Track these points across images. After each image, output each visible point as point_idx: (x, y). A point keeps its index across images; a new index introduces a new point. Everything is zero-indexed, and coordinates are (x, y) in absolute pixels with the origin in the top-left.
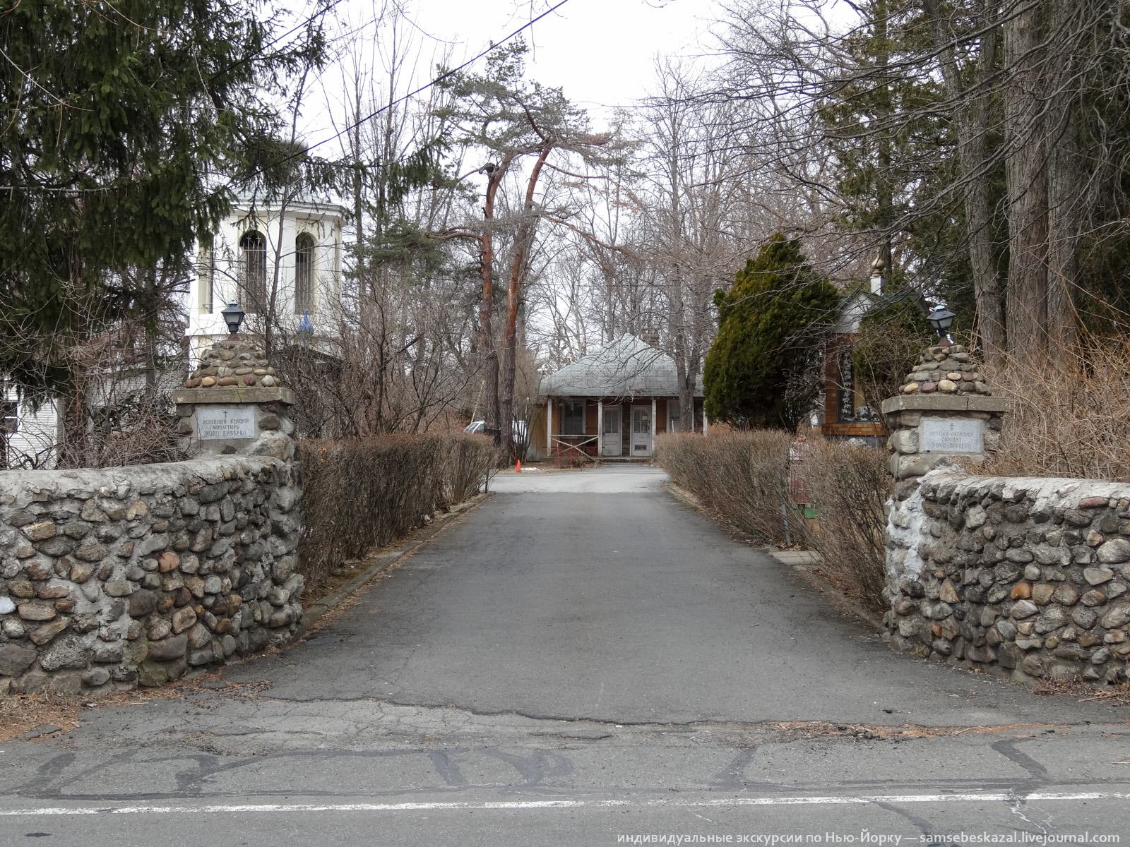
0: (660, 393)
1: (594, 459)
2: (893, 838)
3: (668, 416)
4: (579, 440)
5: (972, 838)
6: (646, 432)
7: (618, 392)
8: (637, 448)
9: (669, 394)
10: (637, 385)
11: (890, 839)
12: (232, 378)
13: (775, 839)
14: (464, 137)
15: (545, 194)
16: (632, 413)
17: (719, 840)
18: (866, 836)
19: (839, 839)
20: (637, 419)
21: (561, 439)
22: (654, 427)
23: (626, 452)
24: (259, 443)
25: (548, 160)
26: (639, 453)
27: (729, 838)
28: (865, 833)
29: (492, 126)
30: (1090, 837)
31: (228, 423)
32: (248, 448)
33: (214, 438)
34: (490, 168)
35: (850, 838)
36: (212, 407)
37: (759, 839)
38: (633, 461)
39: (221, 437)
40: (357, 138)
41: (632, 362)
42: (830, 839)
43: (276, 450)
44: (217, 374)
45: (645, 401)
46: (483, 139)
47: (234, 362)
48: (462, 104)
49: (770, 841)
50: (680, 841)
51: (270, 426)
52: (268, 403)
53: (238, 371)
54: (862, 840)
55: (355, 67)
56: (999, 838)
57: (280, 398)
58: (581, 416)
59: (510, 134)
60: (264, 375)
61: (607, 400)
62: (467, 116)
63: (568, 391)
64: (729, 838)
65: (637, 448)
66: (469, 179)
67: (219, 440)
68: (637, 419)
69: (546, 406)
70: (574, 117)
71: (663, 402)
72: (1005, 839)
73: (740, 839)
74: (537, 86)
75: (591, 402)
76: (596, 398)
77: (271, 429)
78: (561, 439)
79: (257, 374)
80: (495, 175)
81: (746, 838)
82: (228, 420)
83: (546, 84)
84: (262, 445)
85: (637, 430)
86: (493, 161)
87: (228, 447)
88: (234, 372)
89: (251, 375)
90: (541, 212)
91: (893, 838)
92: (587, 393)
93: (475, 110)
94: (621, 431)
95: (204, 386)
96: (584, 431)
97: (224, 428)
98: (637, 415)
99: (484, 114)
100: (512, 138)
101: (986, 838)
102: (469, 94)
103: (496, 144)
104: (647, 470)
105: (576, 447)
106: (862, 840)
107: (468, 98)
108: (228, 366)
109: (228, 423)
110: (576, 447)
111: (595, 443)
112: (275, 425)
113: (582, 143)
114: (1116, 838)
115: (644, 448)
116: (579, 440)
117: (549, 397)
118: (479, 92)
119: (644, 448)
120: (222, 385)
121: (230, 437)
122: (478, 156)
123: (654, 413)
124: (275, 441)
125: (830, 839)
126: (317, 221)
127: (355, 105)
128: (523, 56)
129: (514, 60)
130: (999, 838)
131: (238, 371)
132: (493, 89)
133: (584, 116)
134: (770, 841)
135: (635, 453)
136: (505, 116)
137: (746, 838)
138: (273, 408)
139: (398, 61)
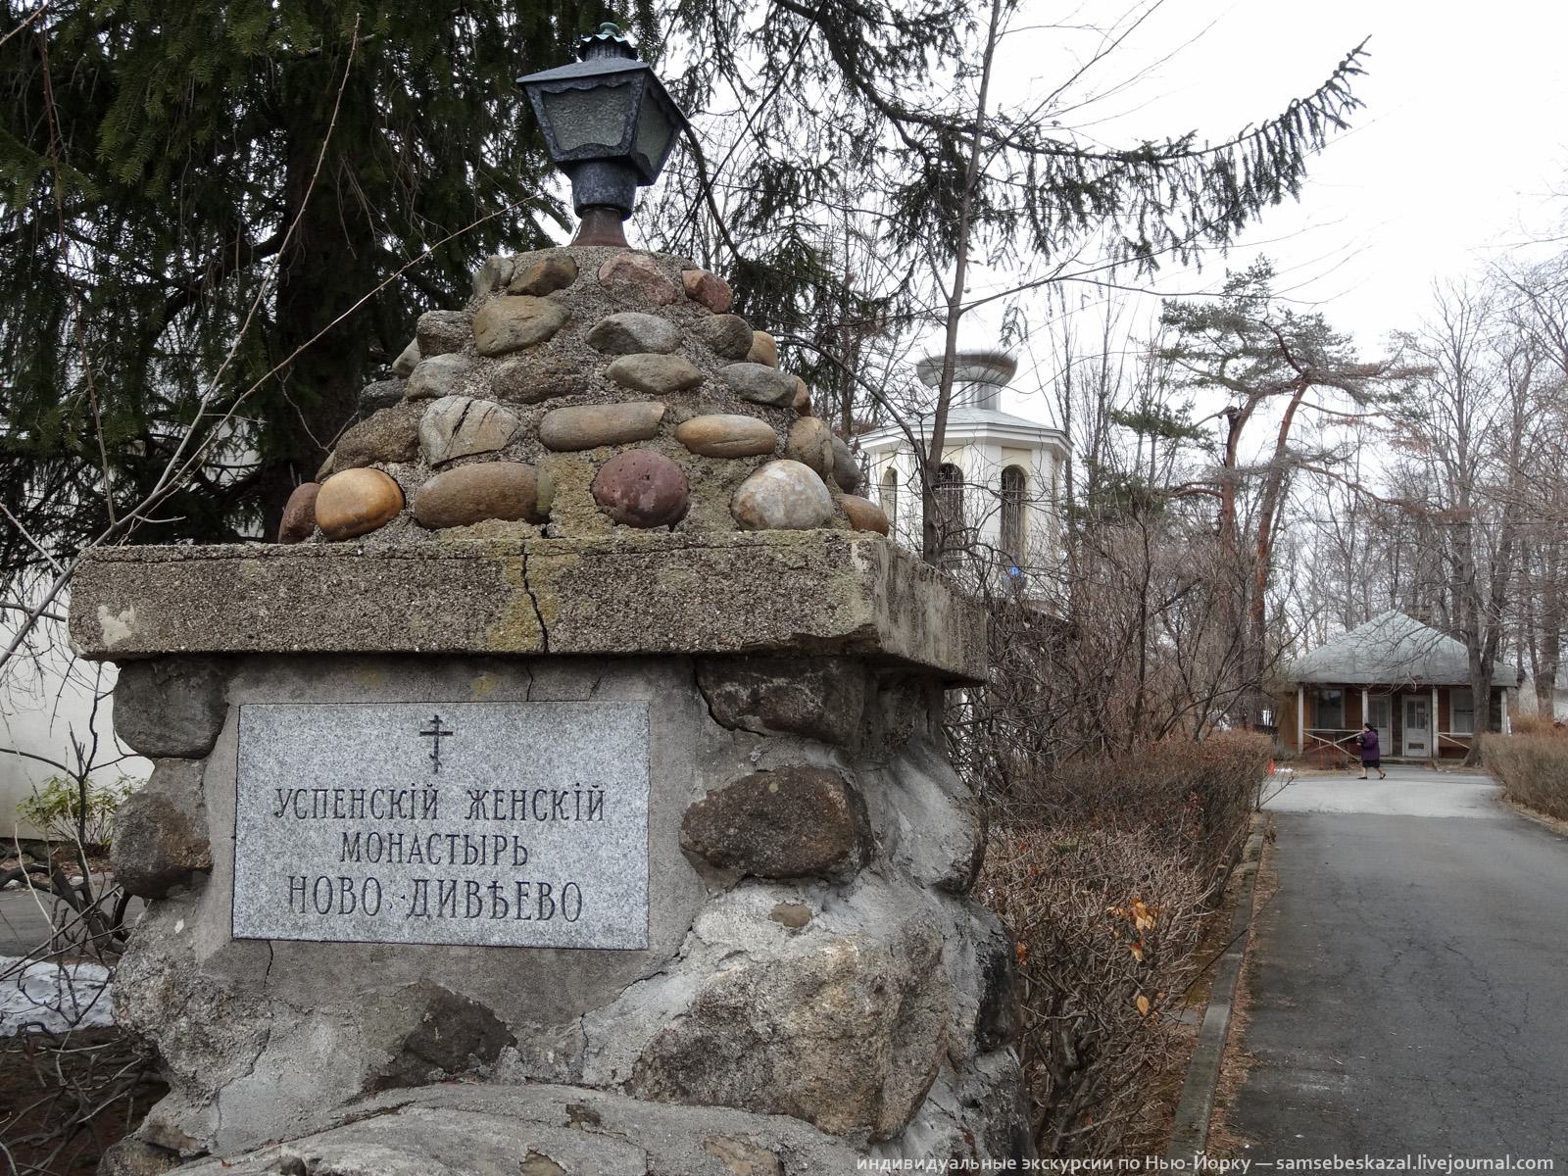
0: (1443, 681)
3: (1452, 708)
4: (1337, 736)
6: (1423, 727)
7: (1387, 680)
8: (1412, 746)
9: (1455, 682)
10: (1410, 673)
12: (509, 471)
14: (1197, 378)
15: (1305, 436)
21: (1315, 734)
22: (1436, 723)
23: (1397, 751)
24: (678, 991)
25: (1304, 398)
29: (1232, 363)
31: (452, 818)
32: (598, 1025)
33: (342, 928)
34: (1230, 411)
36: (340, 686)
38: (1409, 763)
39: (396, 926)
40: (1067, 403)
41: (1406, 644)
43: (819, 1063)
44: (412, 450)
45: (1425, 690)
46: (1222, 380)
47: (539, 364)
48: (1195, 342)
51: (771, 849)
52: (757, 659)
53: (560, 420)
55: (1065, 328)
57: (858, 614)
58: (1339, 707)
59: (1255, 371)
60: (764, 453)
61: (1376, 689)
62: (1202, 356)
63: (1324, 676)
65: (1412, 746)
66: (1204, 426)
67: (380, 952)
69: (1297, 694)
70: (1335, 348)
71: (1445, 691)
74: (1289, 314)
75: (1352, 691)
76: (1363, 685)
77: (784, 878)
78: (1315, 734)
79: (703, 448)
80: (1236, 420)
82: (454, 791)
83: (1299, 311)
84: (707, 1009)
85: (1411, 725)
86: (1235, 403)
87: (444, 1007)
88: (531, 436)
89: (651, 454)
90: (1298, 461)
92: (1347, 680)
93: (1210, 348)
94: (1390, 726)
95: (332, 534)
96: (1343, 725)
97: (421, 852)
98: (1411, 706)
99: (1221, 352)
100: (1257, 375)
102: (1202, 328)
103: (1238, 386)
104: (1434, 776)
107: (1202, 334)
108: (502, 394)
109: (452, 818)
112: (817, 846)
113: (1352, 378)
115: (1421, 746)
117: (1300, 683)
118: (1216, 326)
119: (1421, 746)
120: (432, 521)
121: (460, 927)
122: (1220, 398)
123: (1435, 705)
124: (810, 988)
126: (1027, 448)
128: (1270, 282)
129: (1257, 286)
131: (560, 420)
132: (1233, 322)
133: (1349, 346)
135: (1406, 751)
136: (1247, 352)
138: (805, 700)
139: (1112, 321)
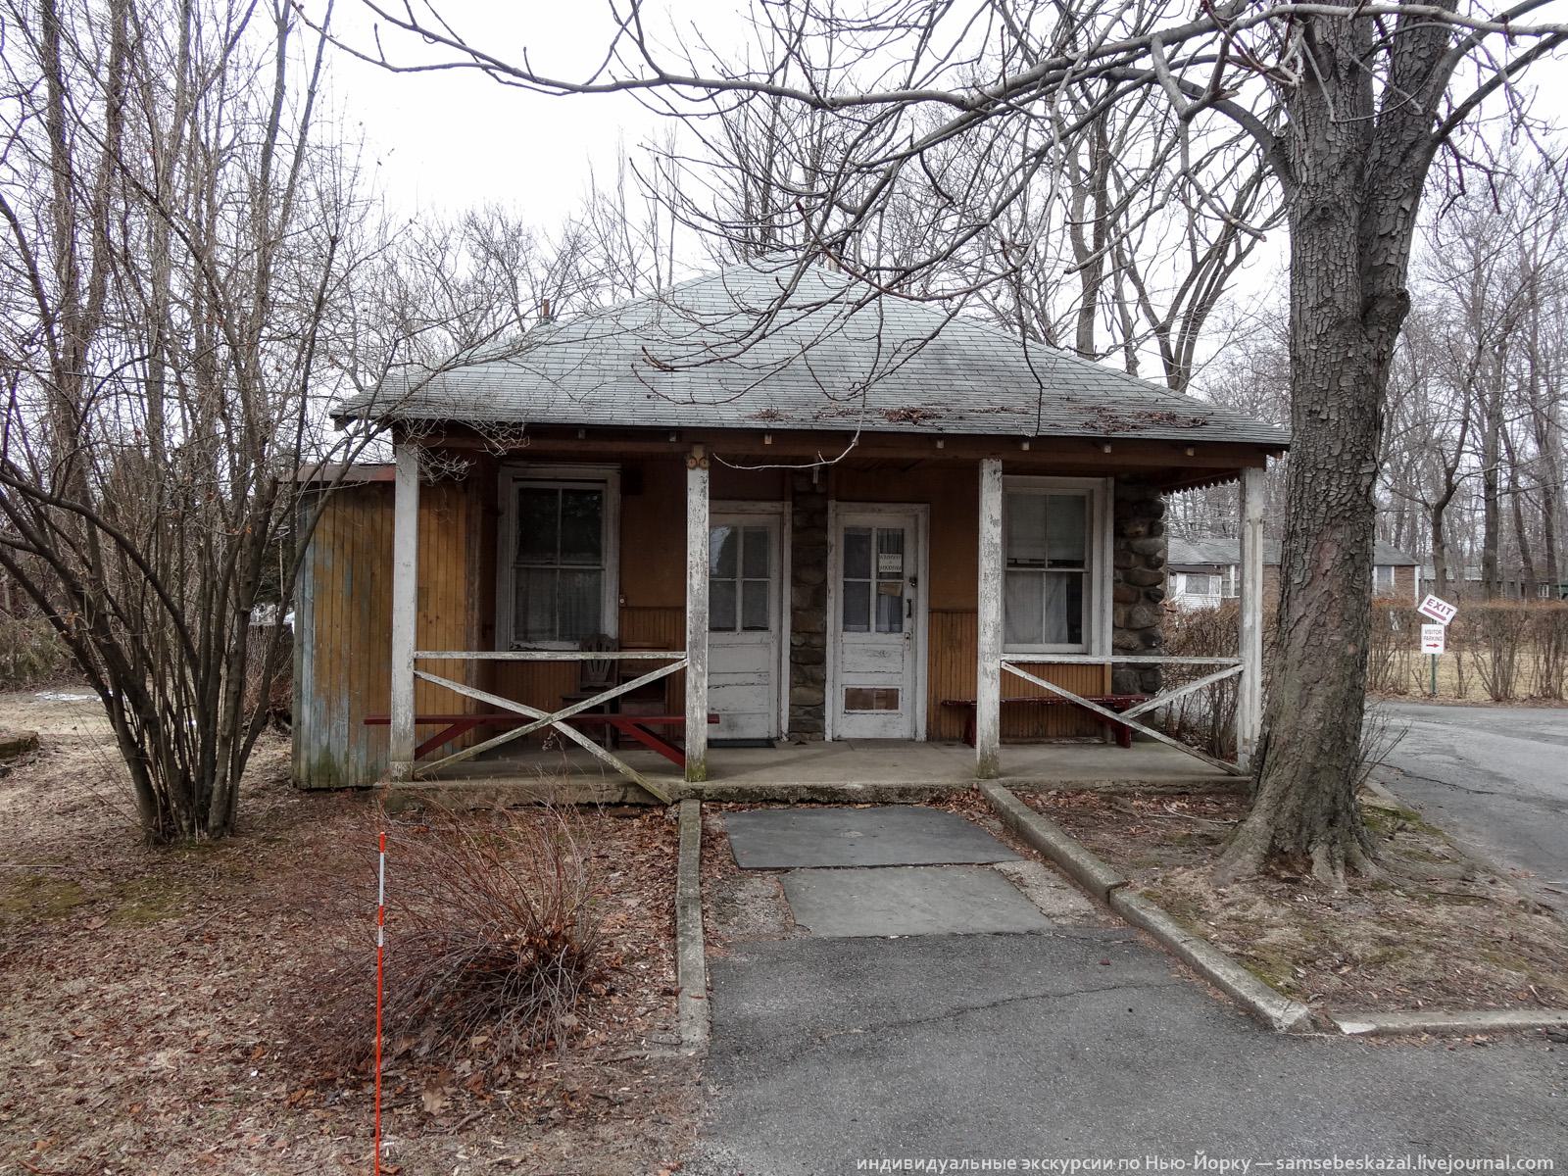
1: (660, 785)
2: (1240, 1163)
5: (1349, 1164)
6: (147, 840)
8: (857, 700)
11: (1235, 1164)
13: (1075, 1164)
16: (835, 540)
17: (998, 1166)
18: (1201, 1161)
19: (1164, 1166)
20: (857, 563)
26: (867, 724)
27: (1012, 1164)
28: (1200, 1158)
30: (1513, 1161)
35: (1180, 1164)
37: (1053, 1165)
42: (1152, 1166)
49: (1069, 1169)
50: (943, 1167)
54: (1196, 1167)
56: (1387, 1163)
64: (1012, 1164)
65: (857, 700)
68: (857, 563)
72: (1394, 1165)
73: (1027, 1164)
78: (491, 676)
81: (1035, 1164)
85: (855, 617)
91: (1240, 1163)
96: (610, 626)
101: (1369, 1164)
105: (557, 721)
106: (1196, 1167)
110: (557, 721)
111: (669, 692)
114: (1548, 1163)
116: (585, 680)
125: (1152, 1166)
127: (311, 77)
130: (1387, 1163)
134: (1069, 1169)
137: (1035, 1164)
